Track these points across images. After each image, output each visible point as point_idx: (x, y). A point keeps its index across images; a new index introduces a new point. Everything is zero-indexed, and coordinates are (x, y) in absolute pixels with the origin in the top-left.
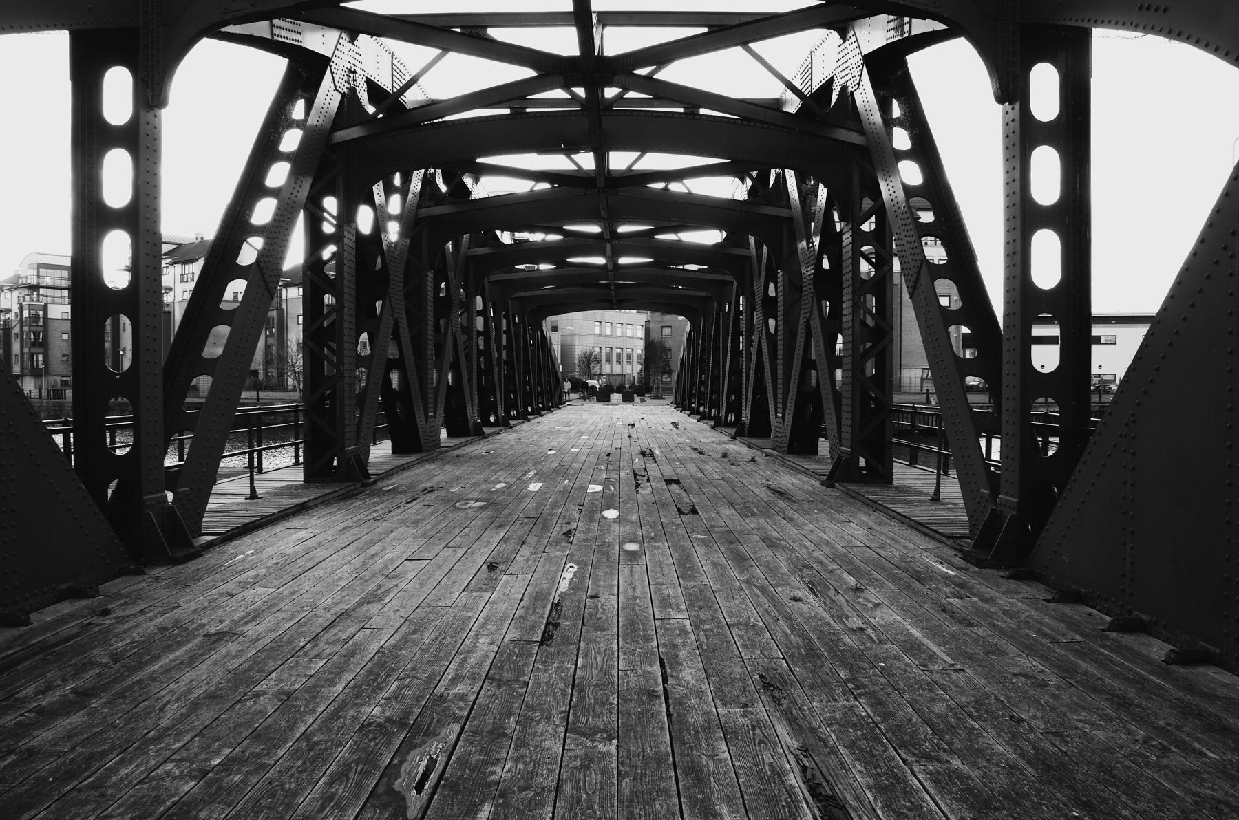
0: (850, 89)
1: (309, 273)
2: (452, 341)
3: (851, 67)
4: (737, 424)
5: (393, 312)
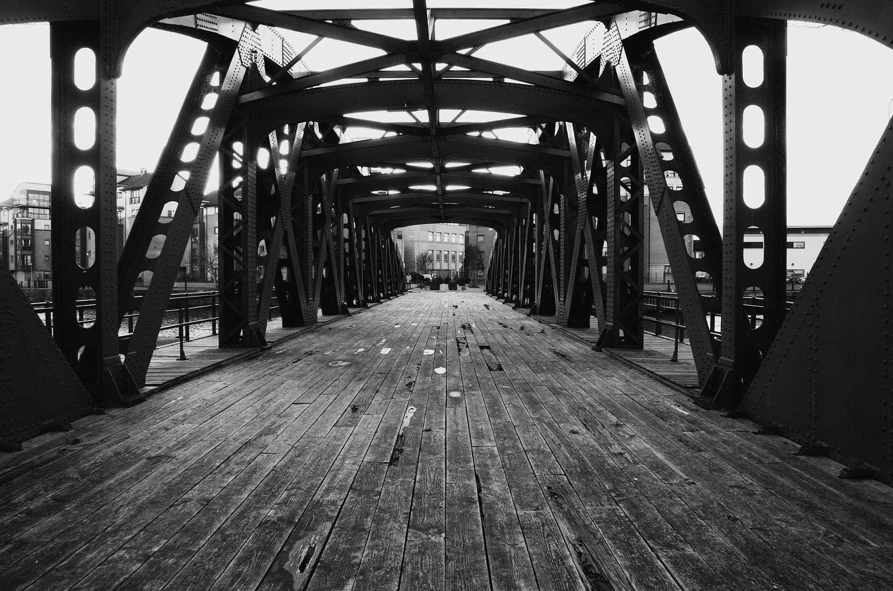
0: (613, 64)
1: (223, 197)
2: (326, 246)
3: (613, 49)
4: (531, 305)
5: (283, 222)
